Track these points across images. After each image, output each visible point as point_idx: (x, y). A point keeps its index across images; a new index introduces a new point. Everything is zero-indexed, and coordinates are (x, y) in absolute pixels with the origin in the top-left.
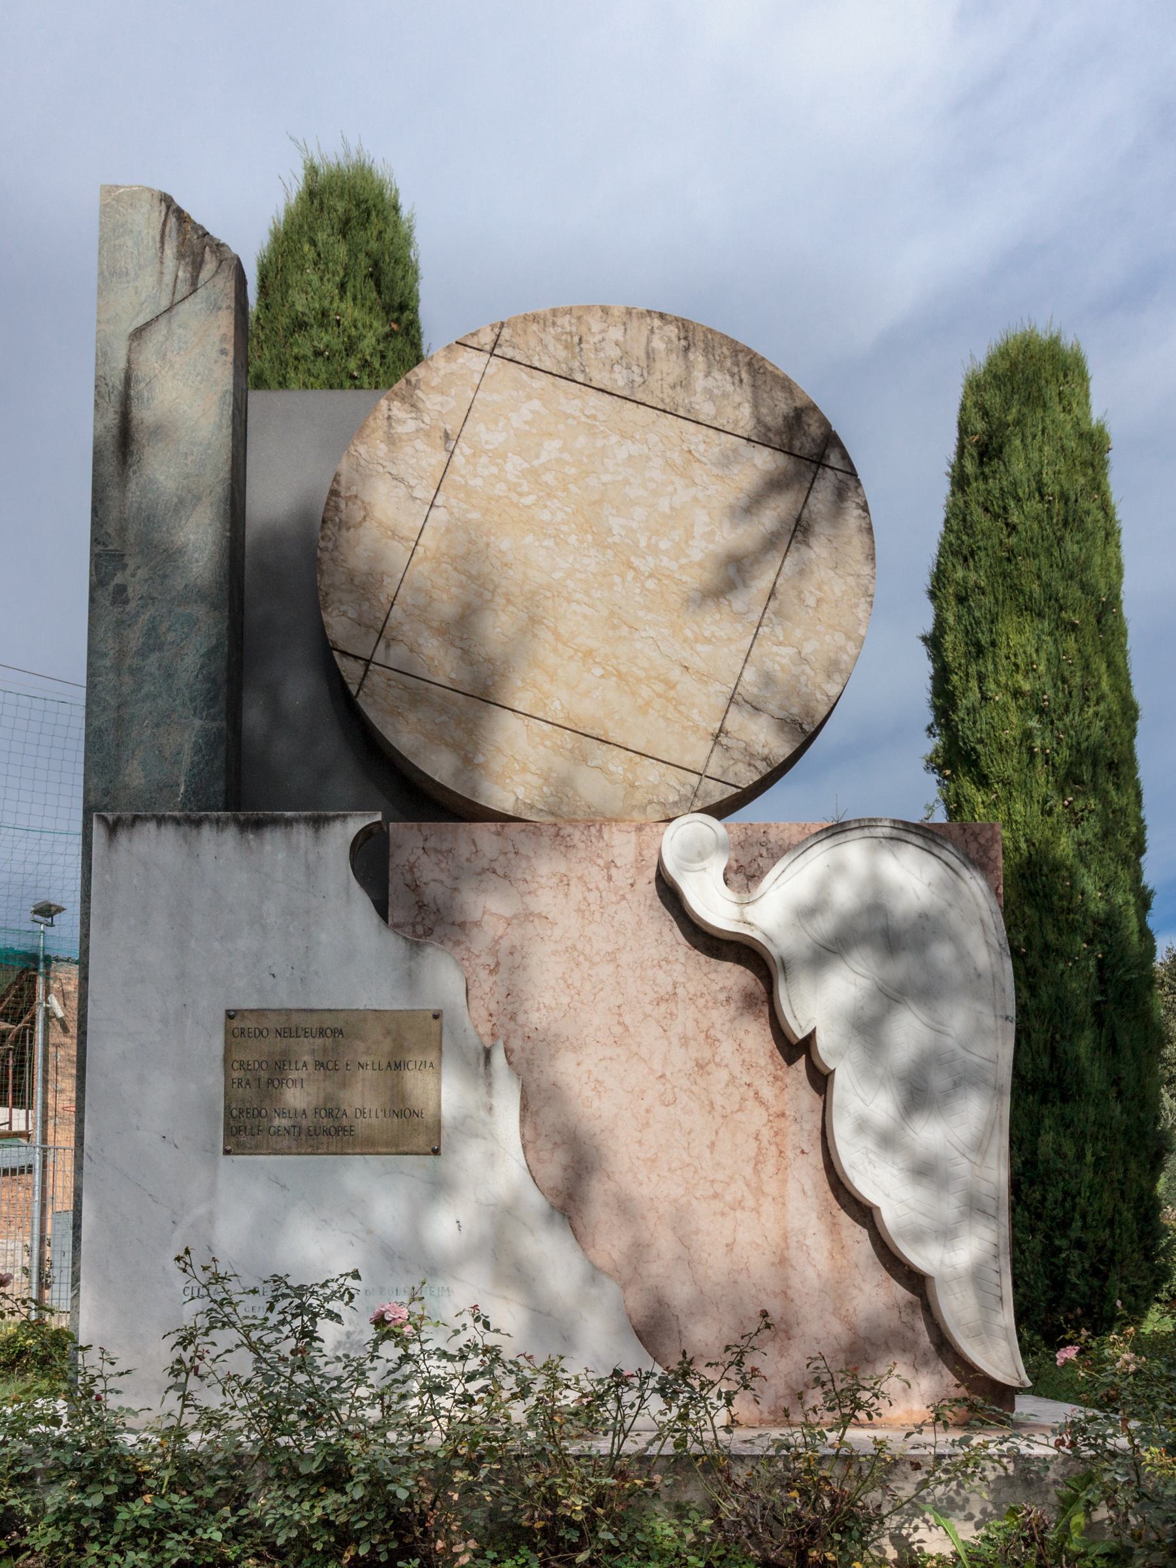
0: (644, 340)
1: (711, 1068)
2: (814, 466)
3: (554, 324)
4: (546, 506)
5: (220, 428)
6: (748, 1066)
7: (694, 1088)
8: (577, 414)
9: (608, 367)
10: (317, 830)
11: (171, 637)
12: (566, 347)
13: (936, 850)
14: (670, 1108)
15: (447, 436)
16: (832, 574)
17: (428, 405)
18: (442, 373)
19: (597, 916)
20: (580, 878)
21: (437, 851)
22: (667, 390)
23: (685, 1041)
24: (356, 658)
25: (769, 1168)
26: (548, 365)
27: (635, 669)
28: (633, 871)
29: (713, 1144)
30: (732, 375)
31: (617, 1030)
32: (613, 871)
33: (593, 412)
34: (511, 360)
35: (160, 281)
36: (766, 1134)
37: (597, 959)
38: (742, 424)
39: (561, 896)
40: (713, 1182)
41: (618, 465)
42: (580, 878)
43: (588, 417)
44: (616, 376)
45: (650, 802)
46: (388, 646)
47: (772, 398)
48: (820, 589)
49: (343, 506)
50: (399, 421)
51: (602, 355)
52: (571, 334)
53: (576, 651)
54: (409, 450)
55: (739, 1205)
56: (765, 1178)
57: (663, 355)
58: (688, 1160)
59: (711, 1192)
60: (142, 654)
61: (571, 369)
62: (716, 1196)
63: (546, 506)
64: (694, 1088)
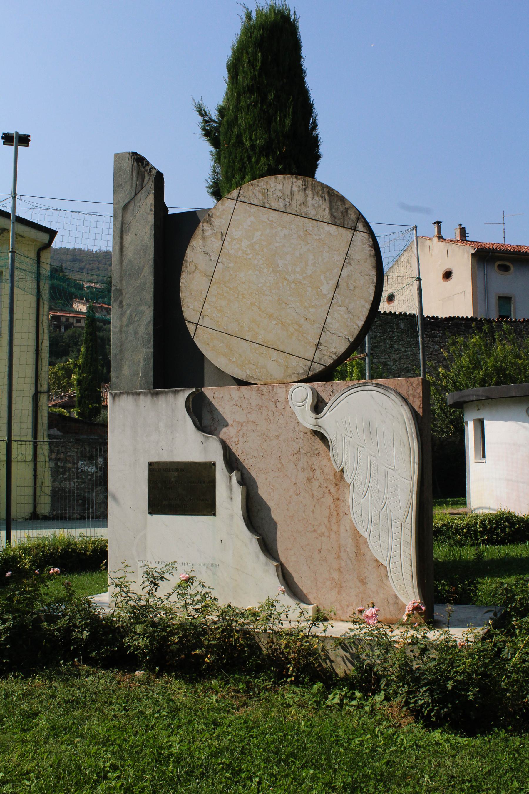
0: (290, 188)
1: (313, 480)
2: (352, 232)
3: (258, 185)
4: (256, 258)
5: (150, 239)
6: (326, 480)
7: (307, 488)
8: (266, 220)
9: (277, 200)
10: (175, 396)
11: (137, 318)
12: (262, 195)
13: (388, 394)
14: (298, 496)
15: (222, 234)
16: (359, 275)
17: (216, 223)
18: (220, 210)
19: (272, 421)
20: (266, 406)
21: (217, 398)
22: (298, 207)
23: (303, 470)
24: (193, 323)
25: (334, 520)
26: (256, 202)
27: (287, 320)
28: (284, 403)
29: (313, 510)
30: (322, 198)
31: (280, 466)
32: (278, 403)
33: (272, 219)
34: (243, 202)
35: (132, 186)
36: (333, 506)
37: (272, 438)
38: (325, 217)
39: (260, 414)
40: (313, 525)
41: (281, 239)
42: (266, 406)
43: (270, 221)
44: (280, 203)
45: (293, 373)
46: (203, 318)
47: (337, 205)
48: (355, 282)
49: (188, 266)
50: (206, 230)
51: (275, 195)
52: (264, 189)
53: (267, 315)
54: (209, 242)
55: (322, 534)
56: (332, 524)
57: (297, 193)
58: (305, 517)
59: (313, 529)
60: (128, 325)
61: (264, 203)
62: (315, 531)
63: (256, 258)
64: (307, 488)
